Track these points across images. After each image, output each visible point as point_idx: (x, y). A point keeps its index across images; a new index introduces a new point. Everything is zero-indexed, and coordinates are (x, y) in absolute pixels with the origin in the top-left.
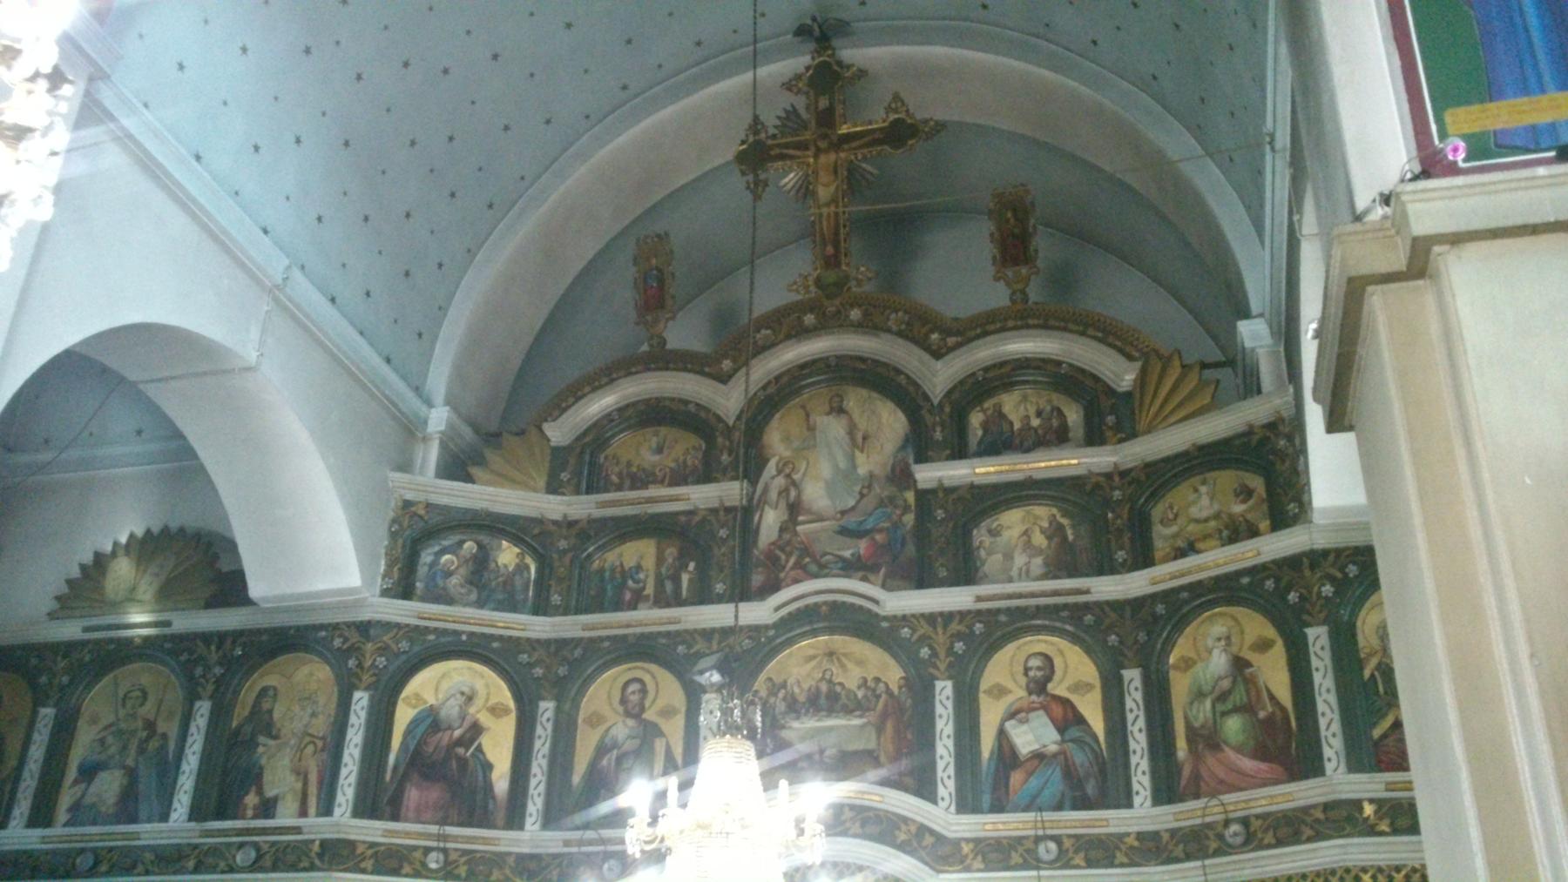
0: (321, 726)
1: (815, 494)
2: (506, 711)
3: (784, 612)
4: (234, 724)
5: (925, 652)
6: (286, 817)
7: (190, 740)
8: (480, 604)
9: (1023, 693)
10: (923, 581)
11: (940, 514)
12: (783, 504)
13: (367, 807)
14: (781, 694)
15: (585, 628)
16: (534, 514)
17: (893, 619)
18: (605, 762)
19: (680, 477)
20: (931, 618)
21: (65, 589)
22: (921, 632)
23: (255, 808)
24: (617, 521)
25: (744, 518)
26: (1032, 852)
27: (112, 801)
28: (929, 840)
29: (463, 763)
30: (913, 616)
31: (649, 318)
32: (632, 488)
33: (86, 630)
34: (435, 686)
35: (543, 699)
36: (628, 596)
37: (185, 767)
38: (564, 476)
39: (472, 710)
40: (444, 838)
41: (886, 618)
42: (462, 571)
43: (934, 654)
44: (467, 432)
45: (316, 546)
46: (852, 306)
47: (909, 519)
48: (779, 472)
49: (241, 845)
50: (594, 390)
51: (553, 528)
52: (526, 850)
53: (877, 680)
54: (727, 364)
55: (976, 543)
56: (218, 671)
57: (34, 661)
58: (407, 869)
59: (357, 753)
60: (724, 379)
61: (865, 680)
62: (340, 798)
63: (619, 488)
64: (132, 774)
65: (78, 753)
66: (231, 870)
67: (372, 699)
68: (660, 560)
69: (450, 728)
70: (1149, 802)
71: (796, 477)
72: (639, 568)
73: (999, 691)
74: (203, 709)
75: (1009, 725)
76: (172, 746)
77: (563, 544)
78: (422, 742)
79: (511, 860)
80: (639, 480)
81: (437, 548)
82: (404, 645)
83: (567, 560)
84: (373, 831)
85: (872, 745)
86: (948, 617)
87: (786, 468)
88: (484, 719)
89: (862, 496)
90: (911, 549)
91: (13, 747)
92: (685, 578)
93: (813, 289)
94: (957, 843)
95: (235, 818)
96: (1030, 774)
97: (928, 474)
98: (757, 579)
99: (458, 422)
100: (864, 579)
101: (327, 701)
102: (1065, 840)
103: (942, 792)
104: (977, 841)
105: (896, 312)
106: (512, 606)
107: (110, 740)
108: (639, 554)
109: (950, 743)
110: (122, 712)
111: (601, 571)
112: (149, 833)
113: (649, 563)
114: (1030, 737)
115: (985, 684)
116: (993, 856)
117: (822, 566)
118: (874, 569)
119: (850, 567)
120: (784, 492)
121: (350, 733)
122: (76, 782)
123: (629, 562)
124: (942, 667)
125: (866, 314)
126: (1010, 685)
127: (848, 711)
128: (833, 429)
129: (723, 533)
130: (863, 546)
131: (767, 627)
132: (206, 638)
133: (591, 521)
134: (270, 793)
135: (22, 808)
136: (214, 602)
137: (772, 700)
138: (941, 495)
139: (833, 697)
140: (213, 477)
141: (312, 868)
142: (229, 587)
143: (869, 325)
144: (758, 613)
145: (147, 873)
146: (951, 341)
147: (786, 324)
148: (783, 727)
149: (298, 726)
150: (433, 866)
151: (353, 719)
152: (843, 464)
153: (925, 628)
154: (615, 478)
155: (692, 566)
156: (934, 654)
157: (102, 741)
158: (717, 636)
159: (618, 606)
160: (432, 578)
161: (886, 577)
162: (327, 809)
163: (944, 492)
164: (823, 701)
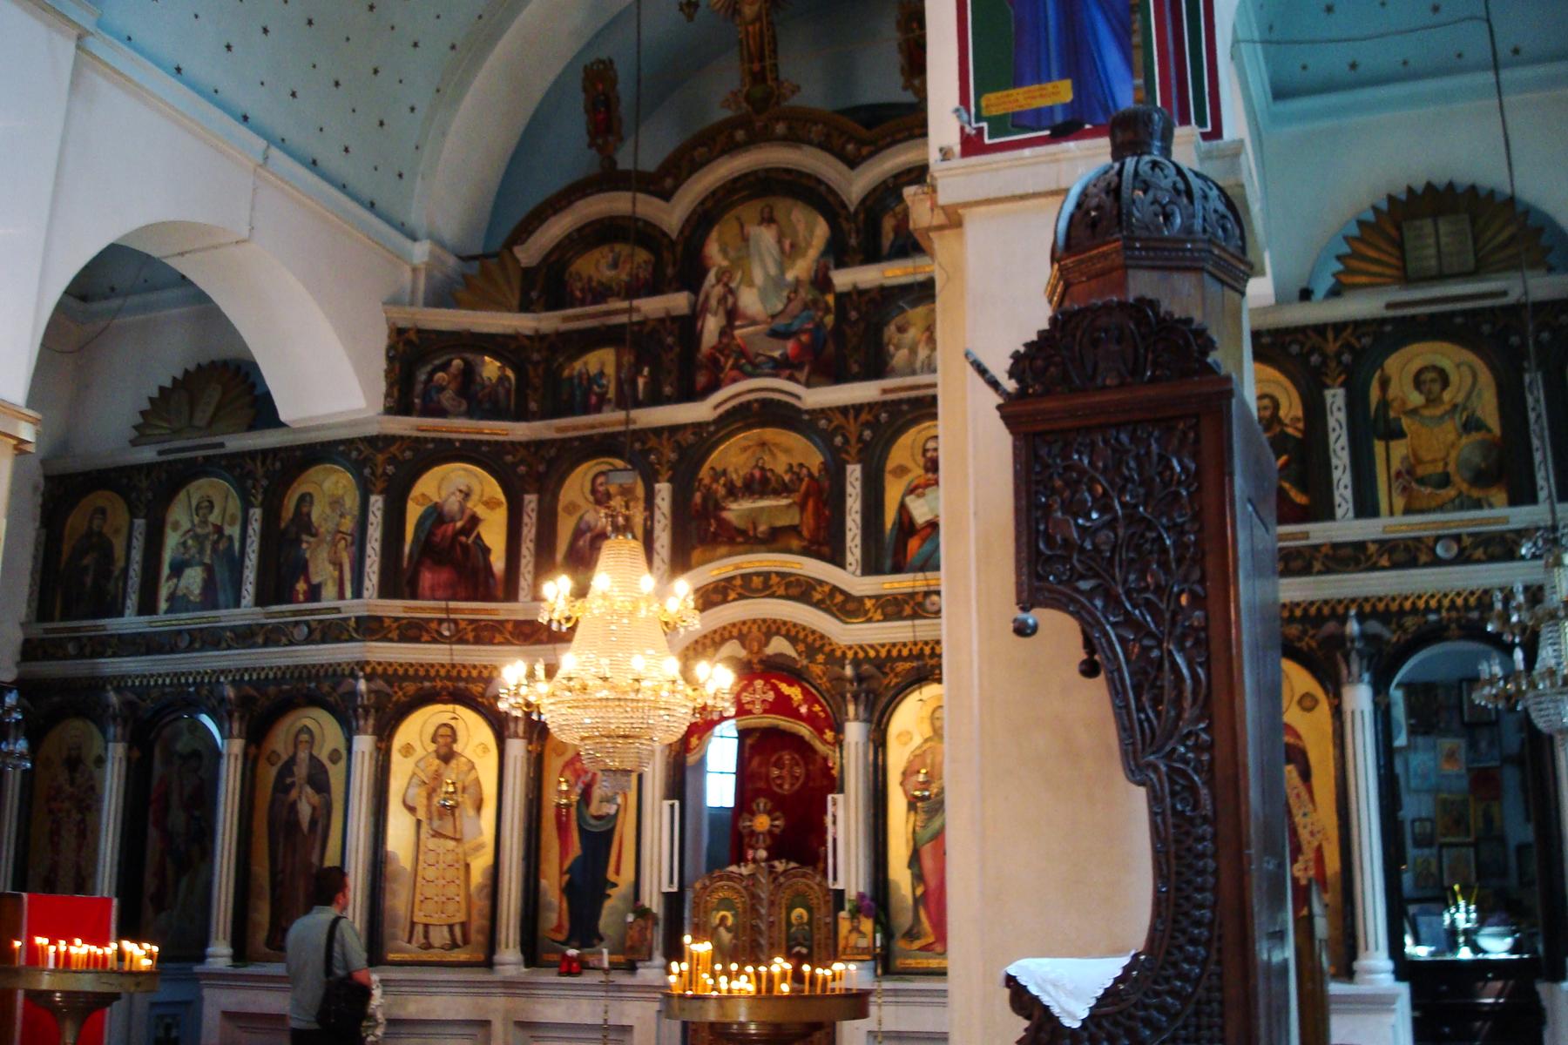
0: (348, 524)
1: (750, 301)
2: (499, 504)
3: (721, 410)
4: (283, 525)
5: (838, 440)
6: (329, 599)
7: (249, 541)
8: (470, 414)
9: (921, 472)
10: (839, 376)
11: (854, 315)
12: (721, 312)
13: (388, 589)
14: (722, 481)
15: (559, 430)
16: (510, 331)
17: (812, 412)
18: (581, 543)
19: (636, 289)
20: (844, 410)
21: (140, 420)
22: (835, 423)
23: (305, 593)
24: (581, 333)
25: (688, 326)
26: (921, 605)
27: (197, 592)
28: (839, 598)
29: (465, 548)
30: (830, 409)
31: (600, 141)
32: (594, 302)
33: (160, 453)
34: (442, 485)
35: (528, 492)
36: (594, 399)
37: (247, 562)
38: (534, 295)
39: (470, 505)
40: (447, 610)
41: (807, 412)
42: (453, 386)
43: (846, 441)
44: (452, 261)
45: (325, 379)
46: (777, 120)
47: (829, 320)
48: (719, 280)
49: (297, 623)
50: (555, 212)
51: (526, 342)
52: (520, 617)
53: (801, 465)
54: (669, 182)
55: (886, 339)
56: (265, 482)
57: (125, 481)
58: (426, 637)
59: (377, 546)
60: (667, 196)
61: (791, 466)
62: (367, 584)
63: (583, 303)
64: (209, 569)
65: (167, 556)
66: (291, 643)
67: (386, 503)
68: (619, 366)
69: (453, 520)
70: (1351, 514)
71: (733, 285)
72: (601, 374)
73: (902, 471)
74: (256, 513)
75: (910, 500)
76: (237, 545)
77: (536, 357)
78: (431, 534)
79: (510, 626)
80: (600, 293)
81: (429, 368)
82: (408, 454)
83: (540, 371)
84: (395, 608)
85: (796, 521)
86: (858, 408)
87: (724, 276)
88: (481, 511)
89: (789, 300)
90: (831, 348)
91: (119, 552)
92: (641, 382)
93: (744, 105)
94: (860, 600)
95: (290, 602)
96: (924, 541)
97: (844, 279)
98: (702, 379)
99: (438, 251)
100: (791, 378)
101: (351, 501)
102: (1465, 538)
103: (850, 558)
104: (877, 597)
105: (816, 123)
106: (497, 412)
107: (190, 542)
108: (601, 361)
109: (858, 518)
110: (196, 520)
111: (571, 378)
112: (114, 625)
113: (610, 370)
114: (926, 509)
115: (891, 464)
116: (890, 609)
117: (756, 366)
118: (799, 366)
119: (781, 367)
120: (722, 300)
121: (371, 530)
122: (169, 578)
123: (593, 369)
124: (853, 451)
125: (790, 128)
126: (910, 464)
127: (777, 493)
128: (766, 237)
129: (670, 340)
130: (790, 346)
131: (708, 424)
132: (252, 454)
133: (560, 335)
134: (315, 580)
135: (132, 601)
136: (252, 427)
137: (714, 486)
138: (855, 297)
139: (764, 481)
140: (141, 249)
141: (352, 639)
142: (263, 411)
143: (793, 139)
144: (699, 411)
145: (229, 647)
146: (865, 151)
147: (717, 141)
148: (724, 509)
149: (331, 526)
150: (447, 633)
151: (372, 518)
152: (773, 270)
153: (838, 420)
154: (578, 294)
155: (646, 371)
156: (846, 441)
157: (184, 544)
158: (666, 435)
159: (586, 410)
160: (426, 394)
161: (810, 374)
162: (358, 594)
163: (858, 293)
164: (756, 486)
